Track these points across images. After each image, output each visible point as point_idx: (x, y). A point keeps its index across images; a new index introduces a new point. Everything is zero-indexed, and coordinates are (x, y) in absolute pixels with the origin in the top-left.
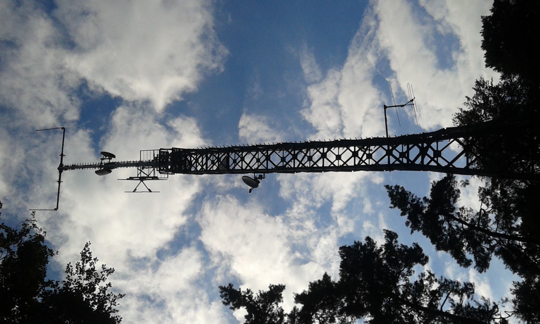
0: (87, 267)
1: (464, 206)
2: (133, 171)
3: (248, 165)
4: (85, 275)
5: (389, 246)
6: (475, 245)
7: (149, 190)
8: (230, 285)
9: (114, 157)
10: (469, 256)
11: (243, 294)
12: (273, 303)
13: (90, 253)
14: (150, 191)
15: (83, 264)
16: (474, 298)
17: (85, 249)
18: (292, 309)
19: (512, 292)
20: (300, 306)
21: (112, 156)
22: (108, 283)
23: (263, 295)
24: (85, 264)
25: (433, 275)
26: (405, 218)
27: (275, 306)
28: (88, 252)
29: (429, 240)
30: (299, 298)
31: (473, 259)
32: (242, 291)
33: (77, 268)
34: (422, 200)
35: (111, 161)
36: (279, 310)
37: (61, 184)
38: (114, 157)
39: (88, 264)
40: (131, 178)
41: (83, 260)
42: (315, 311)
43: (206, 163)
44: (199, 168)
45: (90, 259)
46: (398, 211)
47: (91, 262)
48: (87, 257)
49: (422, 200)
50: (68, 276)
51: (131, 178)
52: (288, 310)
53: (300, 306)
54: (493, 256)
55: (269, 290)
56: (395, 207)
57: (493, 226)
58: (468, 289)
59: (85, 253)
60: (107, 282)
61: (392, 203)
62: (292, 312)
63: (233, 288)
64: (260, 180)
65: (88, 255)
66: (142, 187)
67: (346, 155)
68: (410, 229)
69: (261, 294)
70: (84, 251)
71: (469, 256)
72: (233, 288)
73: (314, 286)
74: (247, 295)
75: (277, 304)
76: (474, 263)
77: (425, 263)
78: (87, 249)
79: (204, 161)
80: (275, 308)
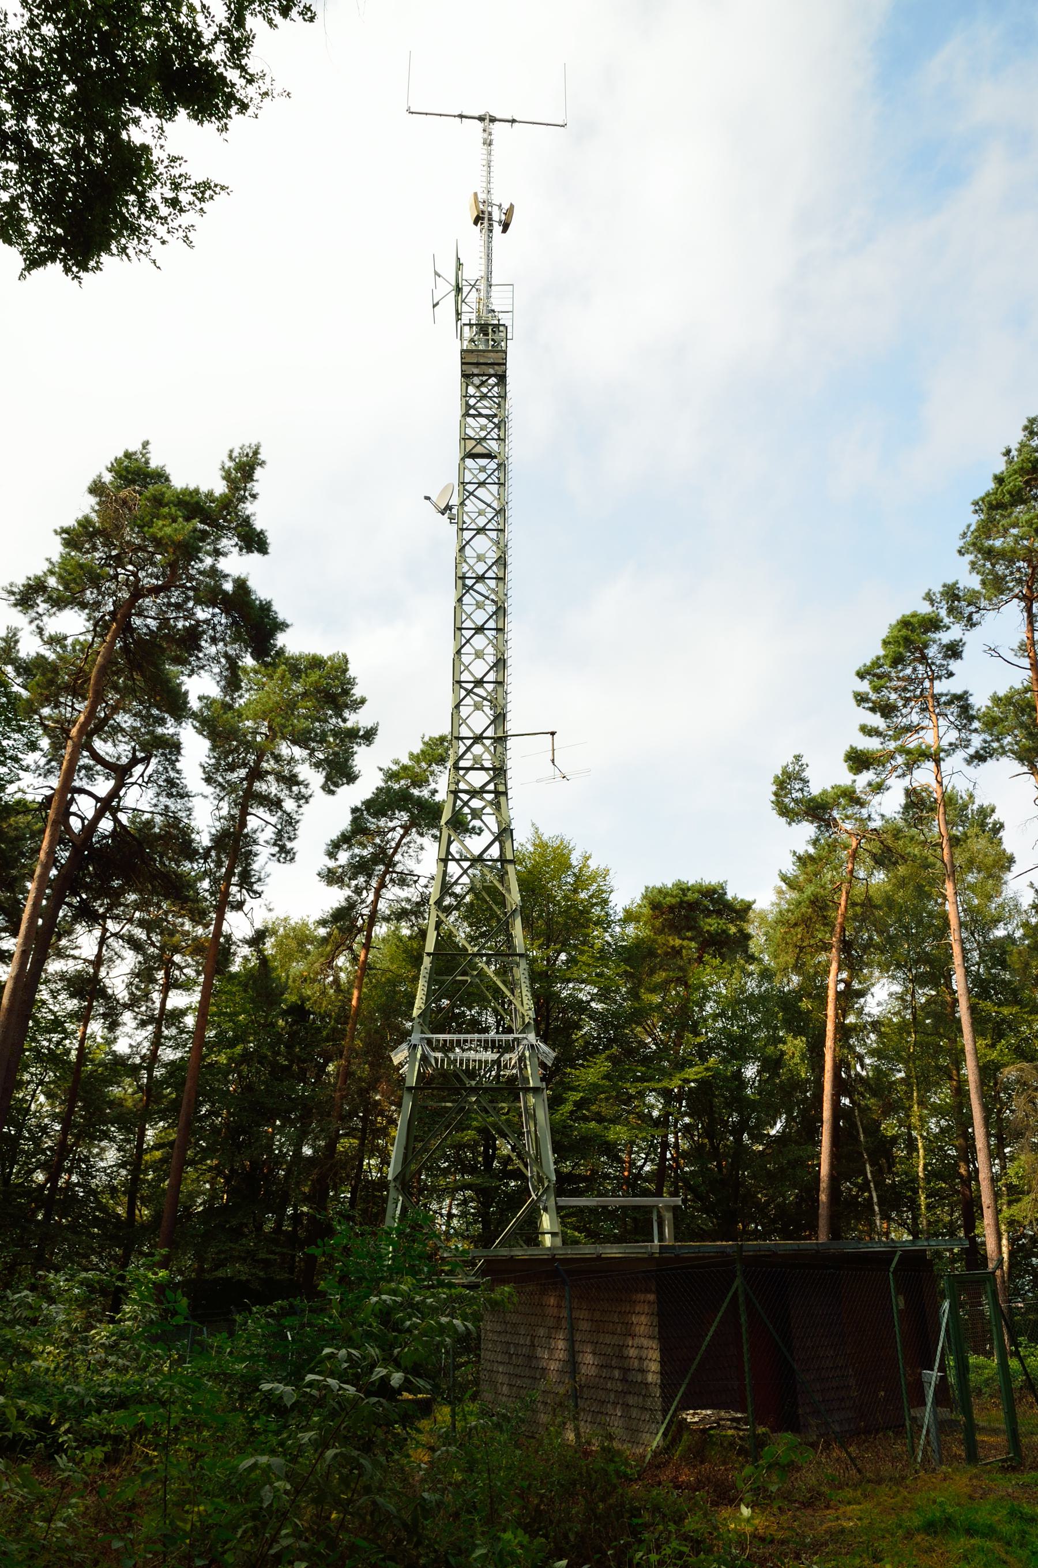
0: (185, 197)
1: (754, 902)
2: (473, 271)
3: (471, 494)
4: (170, 195)
5: (353, 734)
6: (361, 867)
7: (437, 304)
8: (264, 462)
9: (504, 231)
10: (343, 857)
11: (249, 486)
12: (236, 539)
13: (211, 197)
14: (434, 306)
15: (189, 188)
16: (270, 863)
17: (216, 186)
18: (227, 572)
19: (305, 917)
20: (228, 586)
21: (506, 227)
22: (165, 238)
23: (246, 521)
24: (189, 191)
25: (307, 802)
26: (406, 761)
27: (233, 542)
28: (212, 193)
29: (368, 795)
30: (241, 585)
31: (338, 863)
32: (254, 483)
33: (181, 176)
34: (433, 786)
35: (496, 225)
36: (225, 550)
37: (458, 119)
38: (504, 231)
39: (192, 198)
40: (459, 265)
41: (197, 186)
42: (226, 611)
43: (480, 415)
44: (472, 402)
45: (202, 200)
46: (417, 748)
47: (197, 202)
48: (203, 193)
49: (433, 786)
50: (162, 161)
51: (459, 265)
52: (224, 565)
53: (228, 586)
54: (347, 892)
55: (258, 529)
56: (424, 743)
57: (393, 892)
58: (285, 853)
59: (210, 188)
60: (167, 237)
61: (430, 739)
62: (221, 572)
63: (259, 468)
64: (446, 515)
65: (207, 195)
66: (446, 288)
67: (479, 668)
68: (385, 767)
69: (248, 517)
70: (212, 185)
71: (343, 857)
72: (259, 468)
73: (266, 608)
74: (247, 494)
75: (237, 545)
76: (332, 864)
77: (324, 790)
78: (218, 190)
79: (484, 412)
80: (227, 543)
